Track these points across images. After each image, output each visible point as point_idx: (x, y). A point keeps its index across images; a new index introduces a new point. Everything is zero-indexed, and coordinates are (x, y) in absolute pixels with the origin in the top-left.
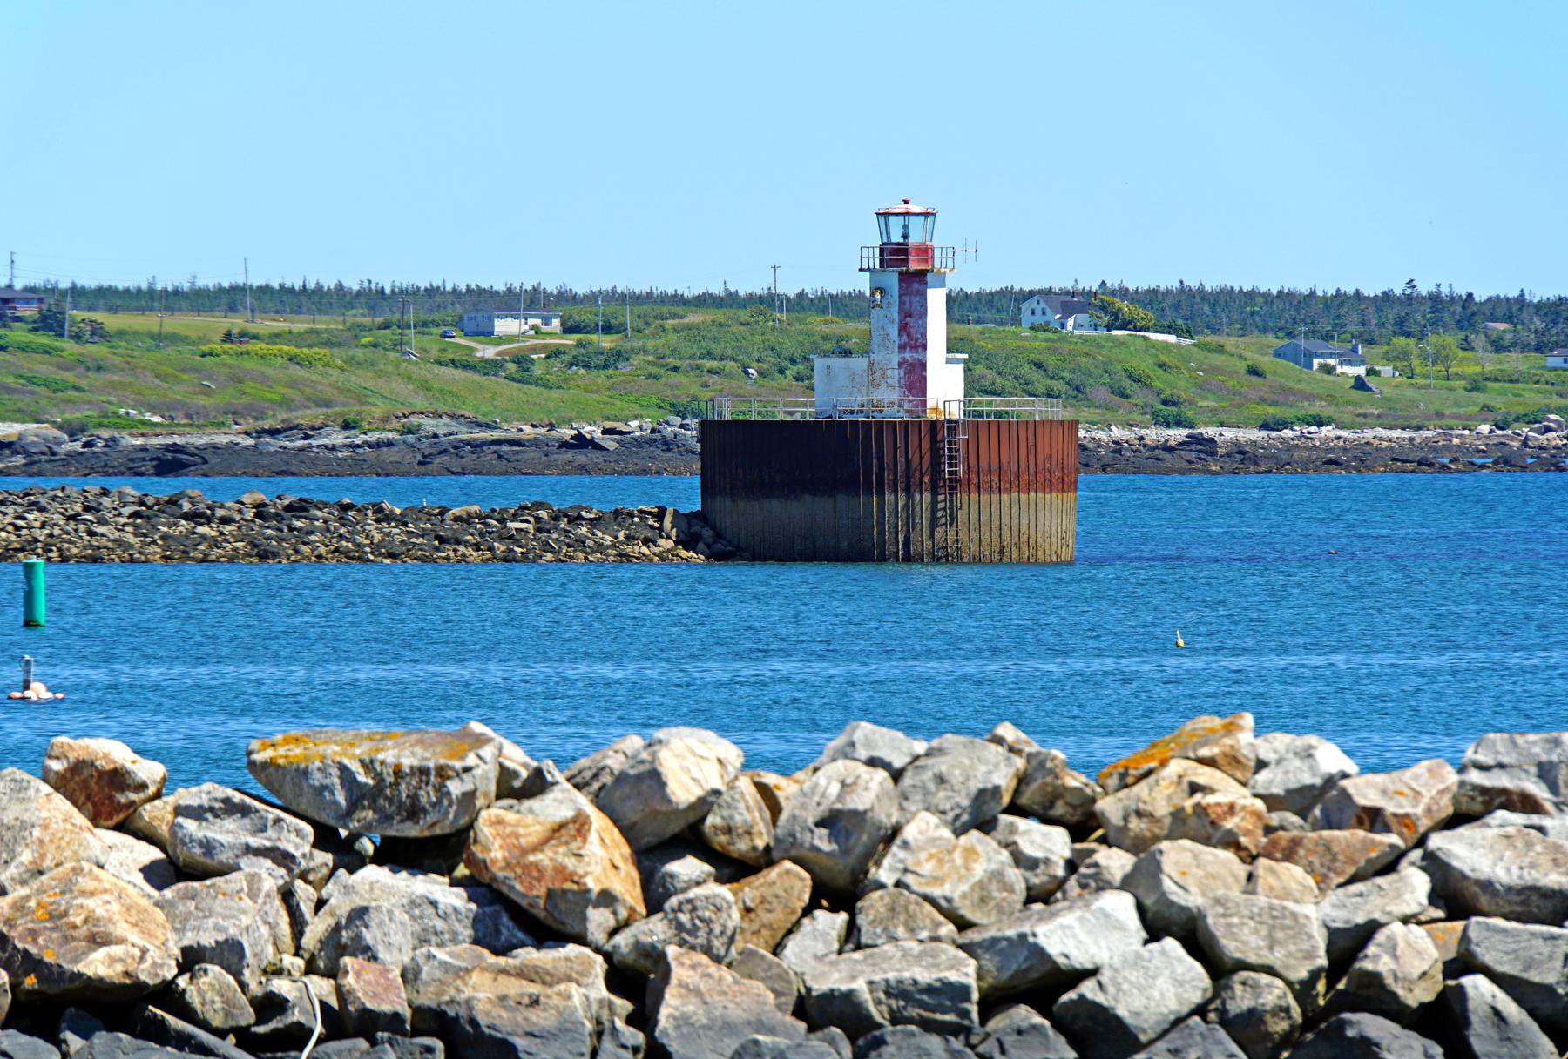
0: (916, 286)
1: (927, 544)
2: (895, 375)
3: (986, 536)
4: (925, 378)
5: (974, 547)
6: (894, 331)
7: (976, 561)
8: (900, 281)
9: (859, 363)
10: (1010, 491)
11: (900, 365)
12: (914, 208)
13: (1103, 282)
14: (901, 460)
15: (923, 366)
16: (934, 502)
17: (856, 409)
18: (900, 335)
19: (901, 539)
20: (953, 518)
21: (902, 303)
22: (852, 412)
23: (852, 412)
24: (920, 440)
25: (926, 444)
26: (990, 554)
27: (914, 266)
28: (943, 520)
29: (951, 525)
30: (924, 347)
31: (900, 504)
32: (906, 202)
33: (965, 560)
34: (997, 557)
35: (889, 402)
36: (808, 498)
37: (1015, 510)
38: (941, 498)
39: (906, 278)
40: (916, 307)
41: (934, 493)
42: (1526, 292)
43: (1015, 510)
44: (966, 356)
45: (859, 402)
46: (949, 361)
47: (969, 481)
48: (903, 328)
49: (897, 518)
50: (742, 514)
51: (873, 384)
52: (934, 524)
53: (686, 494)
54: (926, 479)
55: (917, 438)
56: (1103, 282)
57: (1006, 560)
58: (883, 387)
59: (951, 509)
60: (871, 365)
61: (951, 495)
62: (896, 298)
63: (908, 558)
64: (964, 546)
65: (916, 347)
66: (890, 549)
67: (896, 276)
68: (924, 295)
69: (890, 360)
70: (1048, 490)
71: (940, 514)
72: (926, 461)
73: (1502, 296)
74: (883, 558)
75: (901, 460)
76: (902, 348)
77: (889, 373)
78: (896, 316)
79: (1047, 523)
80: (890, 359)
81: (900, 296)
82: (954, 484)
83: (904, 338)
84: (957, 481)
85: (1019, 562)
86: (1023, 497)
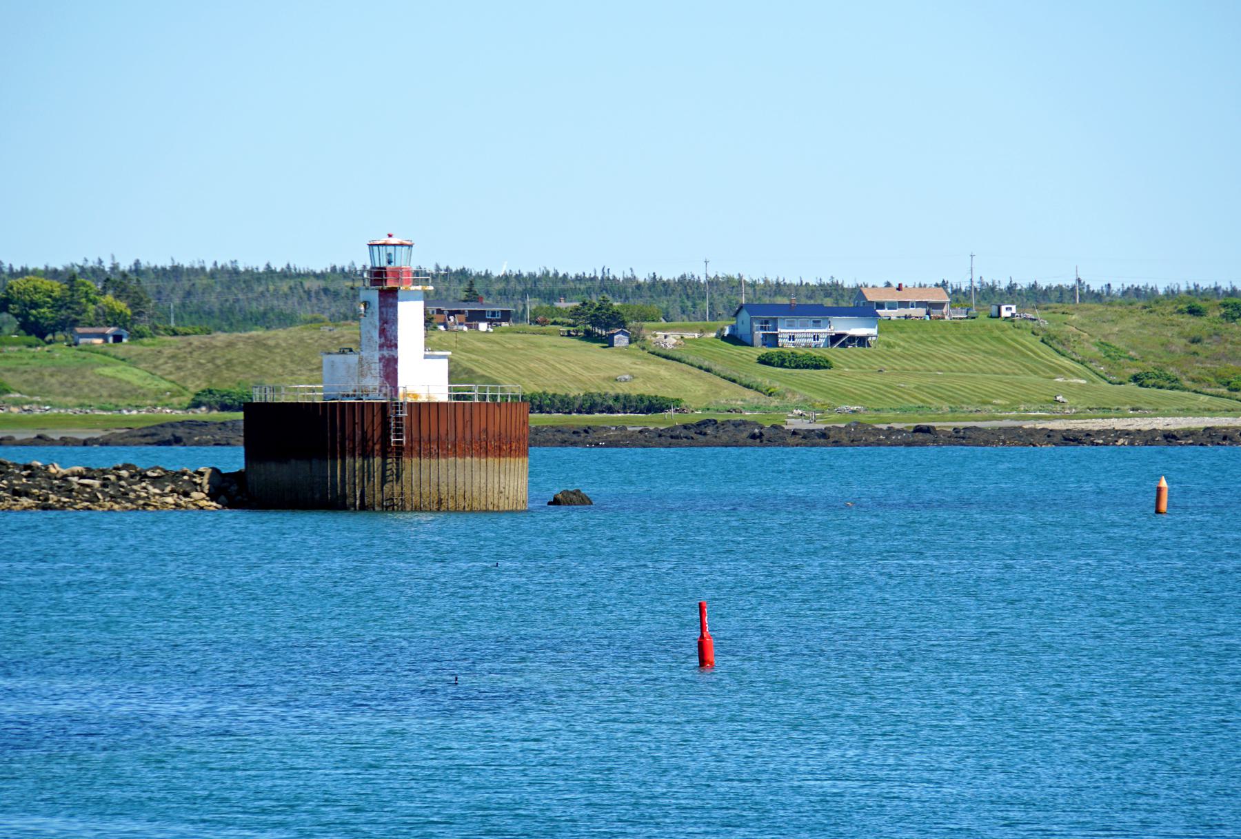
0: (391, 300)
1: (378, 496)
2: (377, 367)
3: (425, 490)
4: (396, 370)
5: (416, 499)
6: (376, 334)
7: (418, 509)
8: (380, 296)
9: (353, 359)
10: (446, 456)
11: (380, 359)
12: (393, 241)
13: (1109, 285)
14: (358, 432)
15: (395, 360)
16: (384, 464)
17: (351, 393)
18: (380, 337)
19: (358, 494)
20: (398, 477)
21: (381, 313)
22: (348, 396)
23: (348, 396)
24: (373, 416)
25: (378, 419)
26: (429, 503)
27: (390, 284)
28: (391, 478)
29: (397, 481)
30: (396, 346)
31: (357, 465)
32: (390, 236)
33: (408, 509)
34: (435, 507)
35: (372, 387)
36: (293, 462)
37: (452, 471)
38: (389, 461)
39: (383, 293)
40: (391, 317)
41: (384, 457)
42: (292, 266)
43: (452, 471)
44: (449, 353)
45: (353, 388)
46: (426, 357)
47: (412, 448)
48: (383, 332)
49: (355, 476)
50: (279, 473)
51: (362, 375)
52: (384, 481)
53: (233, 460)
54: (377, 447)
55: (370, 416)
56: (1109, 285)
57: (443, 508)
58: (369, 377)
59: (397, 470)
60: (361, 360)
61: (397, 459)
62: (377, 309)
63: (363, 507)
64: (406, 497)
65: (391, 346)
66: (349, 501)
67: (377, 293)
68: (395, 306)
69: (373, 356)
70: (483, 455)
71: (388, 473)
72: (377, 434)
73: (159, 267)
74: (403, 509)
75: (358, 432)
76: (381, 346)
77: (373, 366)
78: (377, 324)
79: (483, 481)
80: (373, 355)
81: (380, 308)
82: (399, 451)
83: (383, 340)
84: (402, 449)
85: (456, 511)
86: (459, 461)
